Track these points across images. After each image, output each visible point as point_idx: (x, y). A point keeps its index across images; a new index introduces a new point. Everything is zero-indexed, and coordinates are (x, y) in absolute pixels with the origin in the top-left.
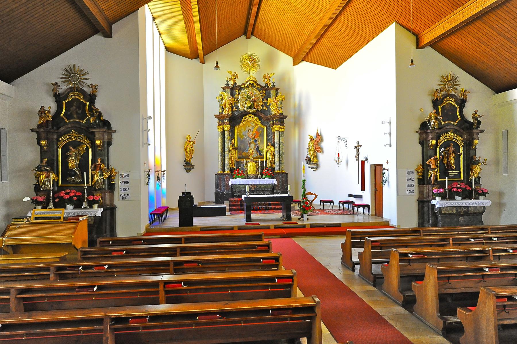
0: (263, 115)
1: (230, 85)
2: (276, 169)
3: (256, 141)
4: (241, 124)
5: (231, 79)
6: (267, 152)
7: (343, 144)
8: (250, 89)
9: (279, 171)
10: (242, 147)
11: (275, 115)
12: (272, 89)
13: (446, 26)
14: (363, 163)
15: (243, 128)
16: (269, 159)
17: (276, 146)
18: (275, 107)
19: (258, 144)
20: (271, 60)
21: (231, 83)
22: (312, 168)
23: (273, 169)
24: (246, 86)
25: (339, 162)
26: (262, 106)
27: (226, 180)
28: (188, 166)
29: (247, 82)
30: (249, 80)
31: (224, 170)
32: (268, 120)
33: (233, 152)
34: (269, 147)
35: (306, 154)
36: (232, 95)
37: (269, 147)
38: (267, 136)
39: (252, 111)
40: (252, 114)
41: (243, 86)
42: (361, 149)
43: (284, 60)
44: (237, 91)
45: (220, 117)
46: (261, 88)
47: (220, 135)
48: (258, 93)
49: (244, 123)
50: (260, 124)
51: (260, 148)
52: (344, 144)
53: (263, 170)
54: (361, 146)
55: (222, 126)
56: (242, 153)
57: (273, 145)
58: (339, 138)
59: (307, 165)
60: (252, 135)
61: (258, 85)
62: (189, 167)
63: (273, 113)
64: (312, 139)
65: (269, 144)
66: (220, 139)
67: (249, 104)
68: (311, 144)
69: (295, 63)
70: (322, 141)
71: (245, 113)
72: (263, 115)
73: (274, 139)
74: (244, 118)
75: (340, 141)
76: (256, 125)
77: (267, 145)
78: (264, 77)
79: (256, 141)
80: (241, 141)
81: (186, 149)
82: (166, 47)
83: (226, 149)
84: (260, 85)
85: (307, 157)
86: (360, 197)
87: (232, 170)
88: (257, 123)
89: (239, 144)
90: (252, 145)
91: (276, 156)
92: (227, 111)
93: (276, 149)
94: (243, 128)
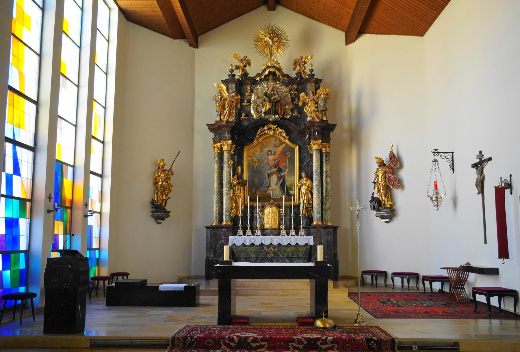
0: (298, 129)
1: (237, 77)
2: (315, 218)
3: (280, 170)
4: (255, 142)
5: (238, 68)
6: (300, 190)
7: (444, 163)
8: (271, 83)
9: (320, 223)
10: (256, 180)
11: (312, 122)
12: (308, 81)
13: (369, 335)
14: (500, 193)
15: (258, 149)
16: (303, 200)
17: (315, 177)
18: (313, 108)
19: (284, 176)
20: (308, 40)
21: (238, 74)
22: (382, 217)
23: (310, 219)
24: (263, 77)
25: (437, 200)
26: (292, 110)
27: (223, 238)
28: (159, 211)
29: (264, 70)
30: (268, 67)
31: (221, 220)
32: (302, 133)
33: (240, 191)
34: (304, 181)
35: (371, 190)
36: (240, 91)
37: (304, 181)
38: (301, 161)
39: (272, 118)
40: (274, 123)
41: (258, 79)
42: (488, 169)
43: (331, 38)
44: (248, 87)
45: (215, 128)
46: (289, 81)
47: (217, 159)
48: (283, 90)
49: (260, 140)
50: (287, 141)
51: (287, 183)
52: (448, 165)
53: (295, 220)
54: (490, 159)
55: (219, 144)
56: (257, 189)
57: (310, 177)
58: (436, 152)
59: (374, 212)
60: (275, 160)
61: (284, 75)
62: (161, 214)
63: (309, 119)
64: (382, 164)
65: (303, 174)
66: (216, 166)
67: (268, 106)
68: (380, 174)
69: (348, 41)
70: (401, 167)
71: (262, 123)
72: (298, 129)
73: (312, 166)
74: (259, 132)
75: (438, 158)
76: (281, 143)
77: (300, 177)
78: (296, 63)
79: (280, 170)
80: (255, 171)
81: (156, 183)
82: (122, 11)
83: (225, 182)
84: (288, 76)
85: (373, 198)
86: (494, 272)
87: (234, 220)
88: (283, 139)
89: (251, 177)
90: (274, 178)
91: (315, 196)
92: (228, 116)
93: (315, 183)
94: (258, 149)
